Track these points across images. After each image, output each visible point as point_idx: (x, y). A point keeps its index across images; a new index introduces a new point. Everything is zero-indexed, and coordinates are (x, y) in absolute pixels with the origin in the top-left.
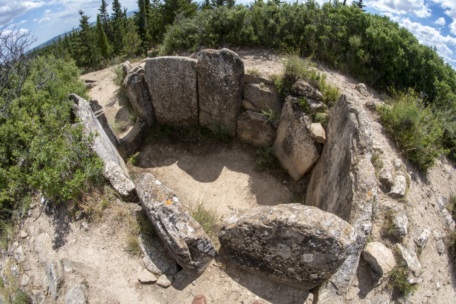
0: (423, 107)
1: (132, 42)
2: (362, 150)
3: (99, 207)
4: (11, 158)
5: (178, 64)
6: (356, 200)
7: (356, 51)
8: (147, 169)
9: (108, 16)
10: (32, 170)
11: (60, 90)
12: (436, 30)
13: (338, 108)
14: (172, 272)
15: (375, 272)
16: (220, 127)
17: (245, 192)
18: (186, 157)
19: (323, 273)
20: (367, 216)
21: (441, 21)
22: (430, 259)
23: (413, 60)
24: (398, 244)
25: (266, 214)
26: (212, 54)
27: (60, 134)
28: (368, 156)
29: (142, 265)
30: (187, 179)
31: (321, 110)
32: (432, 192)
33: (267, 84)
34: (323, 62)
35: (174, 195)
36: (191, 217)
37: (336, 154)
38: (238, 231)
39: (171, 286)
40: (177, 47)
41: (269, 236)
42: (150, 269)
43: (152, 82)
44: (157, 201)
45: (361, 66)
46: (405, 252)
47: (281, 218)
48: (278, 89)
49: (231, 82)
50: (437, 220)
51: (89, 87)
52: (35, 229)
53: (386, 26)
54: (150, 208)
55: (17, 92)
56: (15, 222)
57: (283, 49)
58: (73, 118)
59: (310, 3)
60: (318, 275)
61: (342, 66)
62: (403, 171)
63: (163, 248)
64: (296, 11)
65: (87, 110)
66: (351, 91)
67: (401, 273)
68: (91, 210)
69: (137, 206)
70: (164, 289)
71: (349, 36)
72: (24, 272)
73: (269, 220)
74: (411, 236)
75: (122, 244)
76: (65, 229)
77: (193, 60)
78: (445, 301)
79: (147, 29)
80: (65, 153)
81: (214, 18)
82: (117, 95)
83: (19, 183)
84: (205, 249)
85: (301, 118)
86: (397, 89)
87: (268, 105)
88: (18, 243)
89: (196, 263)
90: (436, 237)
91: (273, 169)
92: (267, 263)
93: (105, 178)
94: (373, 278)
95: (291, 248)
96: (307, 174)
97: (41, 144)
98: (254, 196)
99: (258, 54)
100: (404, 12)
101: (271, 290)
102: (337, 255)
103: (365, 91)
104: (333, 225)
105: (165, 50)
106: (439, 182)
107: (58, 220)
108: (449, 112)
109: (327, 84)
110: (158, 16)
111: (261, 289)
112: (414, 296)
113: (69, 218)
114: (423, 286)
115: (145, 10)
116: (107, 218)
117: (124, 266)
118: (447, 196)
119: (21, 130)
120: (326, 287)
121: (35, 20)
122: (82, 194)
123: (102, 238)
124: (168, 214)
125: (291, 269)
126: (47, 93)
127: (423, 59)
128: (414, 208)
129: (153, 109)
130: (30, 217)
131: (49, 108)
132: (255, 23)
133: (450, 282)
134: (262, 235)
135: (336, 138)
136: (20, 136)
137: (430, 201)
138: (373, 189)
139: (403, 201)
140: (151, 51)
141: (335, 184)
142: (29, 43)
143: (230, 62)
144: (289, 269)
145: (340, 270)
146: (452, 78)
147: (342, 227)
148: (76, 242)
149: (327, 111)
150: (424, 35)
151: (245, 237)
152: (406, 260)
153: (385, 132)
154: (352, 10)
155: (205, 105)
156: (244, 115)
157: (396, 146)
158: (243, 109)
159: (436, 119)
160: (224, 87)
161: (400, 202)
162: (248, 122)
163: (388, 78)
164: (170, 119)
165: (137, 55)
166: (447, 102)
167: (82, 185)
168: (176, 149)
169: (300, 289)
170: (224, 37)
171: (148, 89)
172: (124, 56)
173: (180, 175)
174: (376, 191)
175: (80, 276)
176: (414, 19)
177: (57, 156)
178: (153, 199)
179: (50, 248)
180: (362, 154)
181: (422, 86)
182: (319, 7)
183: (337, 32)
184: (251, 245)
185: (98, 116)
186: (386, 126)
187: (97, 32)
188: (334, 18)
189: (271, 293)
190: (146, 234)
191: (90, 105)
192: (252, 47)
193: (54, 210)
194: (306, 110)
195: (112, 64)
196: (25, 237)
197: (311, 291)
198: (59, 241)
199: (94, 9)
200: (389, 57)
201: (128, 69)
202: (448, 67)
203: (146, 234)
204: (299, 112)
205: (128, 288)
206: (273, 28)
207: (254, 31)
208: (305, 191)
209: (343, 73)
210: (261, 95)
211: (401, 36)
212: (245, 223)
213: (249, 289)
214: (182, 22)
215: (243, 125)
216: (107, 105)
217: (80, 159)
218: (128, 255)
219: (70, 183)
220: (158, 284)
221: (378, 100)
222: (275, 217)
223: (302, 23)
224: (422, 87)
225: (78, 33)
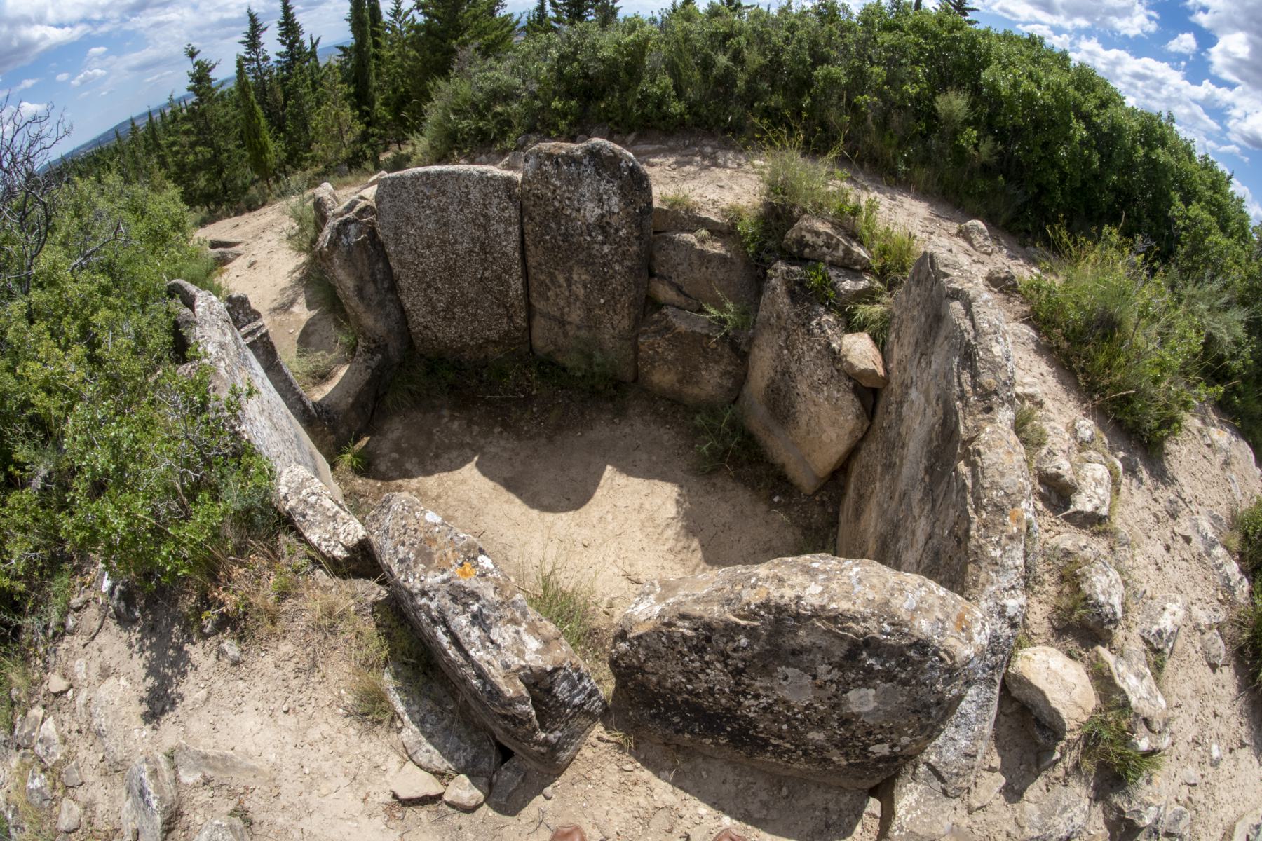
0: (1144, 277)
1: (335, 132)
2: (987, 399)
3: (266, 596)
4: (11, 469)
5: (467, 187)
6: (981, 536)
7: (955, 134)
8: (393, 484)
9: (266, 59)
10: (73, 499)
11: (141, 270)
12: (1173, 68)
13: (915, 290)
14: (484, 765)
15: (1042, 727)
16: (590, 357)
17: (670, 532)
18: (500, 444)
19: (905, 740)
20: (1013, 578)
21: (1183, 44)
22: (1189, 683)
23: (1112, 152)
24: (1100, 649)
25: (738, 588)
26: (562, 156)
27: (145, 395)
28: (1005, 416)
29: (398, 753)
30: (506, 506)
31: (868, 296)
32: (1180, 502)
33: (717, 231)
34: (866, 165)
35: (481, 551)
36: (530, 610)
37: (916, 414)
38: (664, 639)
39: (485, 805)
40: (464, 140)
41: (752, 649)
42: (424, 760)
43: (397, 240)
44: (434, 569)
45: (971, 174)
46: (1121, 669)
47: (782, 597)
48: (748, 244)
49: (617, 231)
50: (1199, 578)
51: (222, 261)
52: (88, 668)
53: (1035, 61)
54: (415, 591)
55: (19, 281)
56: (31, 650)
57: (758, 136)
58: (180, 348)
59: (825, 6)
60: (891, 747)
61: (921, 174)
62: (1099, 452)
63: (456, 700)
64: (788, 29)
65: (220, 323)
66: (945, 241)
67: (1113, 725)
68: (245, 606)
69: (373, 588)
70: (464, 815)
71: (934, 94)
72: (65, 793)
73: (748, 604)
74: (1133, 625)
75: (340, 697)
76: (173, 664)
77: (509, 173)
78: (1237, 793)
79: (377, 94)
80: (164, 447)
81: (563, 57)
82: (300, 280)
83: (37, 540)
84: (574, 697)
85: (814, 323)
86: (1072, 233)
87: (722, 289)
88: (42, 711)
89: (551, 737)
90: (1199, 625)
91: (742, 466)
92: (750, 724)
93: (279, 513)
94: (1037, 745)
95: (815, 677)
96: (840, 473)
97: (97, 425)
98: (695, 544)
99: (687, 151)
100: (1082, 22)
101: (764, 796)
102: (939, 687)
103: (986, 239)
104: (924, 605)
105: (428, 149)
106: (1198, 475)
107: (154, 640)
108: (1216, 286)
109: (880, 227)
110: (405, 57)
111: (737, 795)
112: (1154, 784)
113: (183, 631)
114: (1174, 757)
115: (370, 41)
116: (293, 626)
117: (348, 759)
118: (1223, 511)
119: (35, 386)
120: (914, 777)
121: (62, 77)
122: (217, 560)
123: (280, 683)
124: (466, 605)
125: (817, 736)
126: (105, 280)
127: (1139, 147)
128: (1137, 550)
129: (404, 314)
130: (72, 633)
131: (112, 324)
132: (677, 65)
133: (1246, 741)
134: (731, 646)
135: (913, 372)
136: (33, 405)
137: (1176, 529)
138: (1024, 505)
139: (1105, 532)
140: (389, 155)
141: (917, 495)
142: (48, 142)
143: (613, 176)
144: (810, 736)
145: (950, 730)
146: (1218, 196)
147: (949, 609)
148: (207, 699)
149: (885, 299)
150: (1140, 84)
151: (683, 656)
152: (1126, 688)
153: (1045, 349)
154: (941, 22)
155: (548, 299)
156: (656, 322)
157: (1077, 384)
158: (652, 304)
159: (1182, 308)
160: (597, 246)
161: (1098, 534)
162: (668, 340)
163: (1046, 203)
164: (452, 341)
165: (350, 167)
166: (1207, 259)
167: (216, 536)
168: (470, 423)
169: (842, 790)
170: (591, 108)
171: (385, 258)
172: (316, 169)
173: (486, 495)
174: (1032, 509)
175: (225, 793)
176: (1110, 40)
177: (141, 456)
178: (422, 566)
179: (134, 718)
180: (989, 410)
181: (1138, 219)
182: (851, 15)
183: (903, 82)
184: (701, 676)
185: (250, 339)
186: (1047, 333)
187: (238, 106)
188: (892, 46)
189: (765, 804)
190: (405, 664)
191: (228, 309)
192: (669, 133)
193: (141, 611)
194: (827, 298)
195: (283, 195)
196: (62, 693)
197: (873, 792)
198: (160, 698)
199: (227, 42)
200: (1045, 145)
201: (329, 205)
202: (1207, 166)
203: (405, 664)
204: (807, 304)
205: (364, 820)
206: (727, 79)
207: (675, 87)
208: (834, 523)
209: (923, 194)
210: (702, 264)
211: (1077, 88)
212: (683, 617)
213: (703, 797)
214: (473, 70)
215: (654, 349)
216: (275, 310)
217: (208, 463)
218: (357, 725)
219: (181, 532)
220: (446, 803)
221: (1021, 262)
222: (765, 595)
223: (805, 62)
224: (1139, 222)
225: (185, 111)
